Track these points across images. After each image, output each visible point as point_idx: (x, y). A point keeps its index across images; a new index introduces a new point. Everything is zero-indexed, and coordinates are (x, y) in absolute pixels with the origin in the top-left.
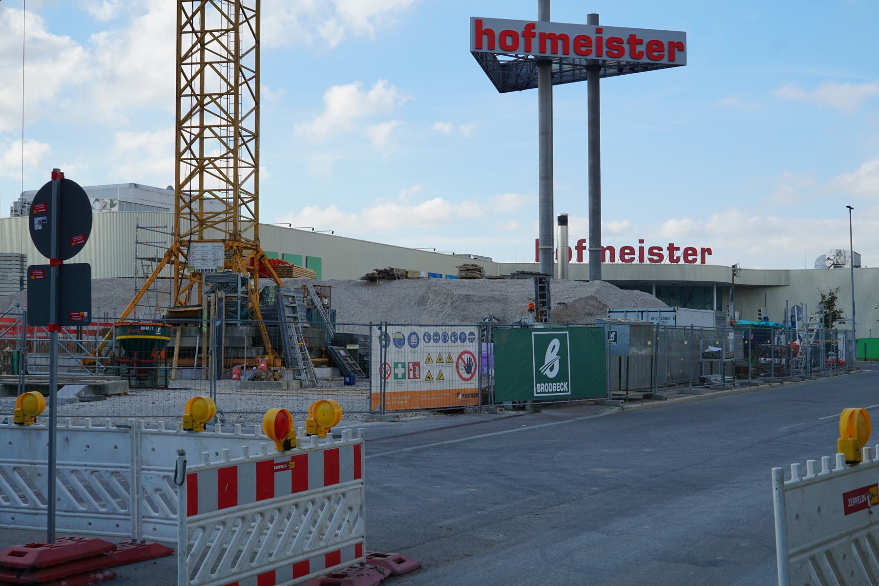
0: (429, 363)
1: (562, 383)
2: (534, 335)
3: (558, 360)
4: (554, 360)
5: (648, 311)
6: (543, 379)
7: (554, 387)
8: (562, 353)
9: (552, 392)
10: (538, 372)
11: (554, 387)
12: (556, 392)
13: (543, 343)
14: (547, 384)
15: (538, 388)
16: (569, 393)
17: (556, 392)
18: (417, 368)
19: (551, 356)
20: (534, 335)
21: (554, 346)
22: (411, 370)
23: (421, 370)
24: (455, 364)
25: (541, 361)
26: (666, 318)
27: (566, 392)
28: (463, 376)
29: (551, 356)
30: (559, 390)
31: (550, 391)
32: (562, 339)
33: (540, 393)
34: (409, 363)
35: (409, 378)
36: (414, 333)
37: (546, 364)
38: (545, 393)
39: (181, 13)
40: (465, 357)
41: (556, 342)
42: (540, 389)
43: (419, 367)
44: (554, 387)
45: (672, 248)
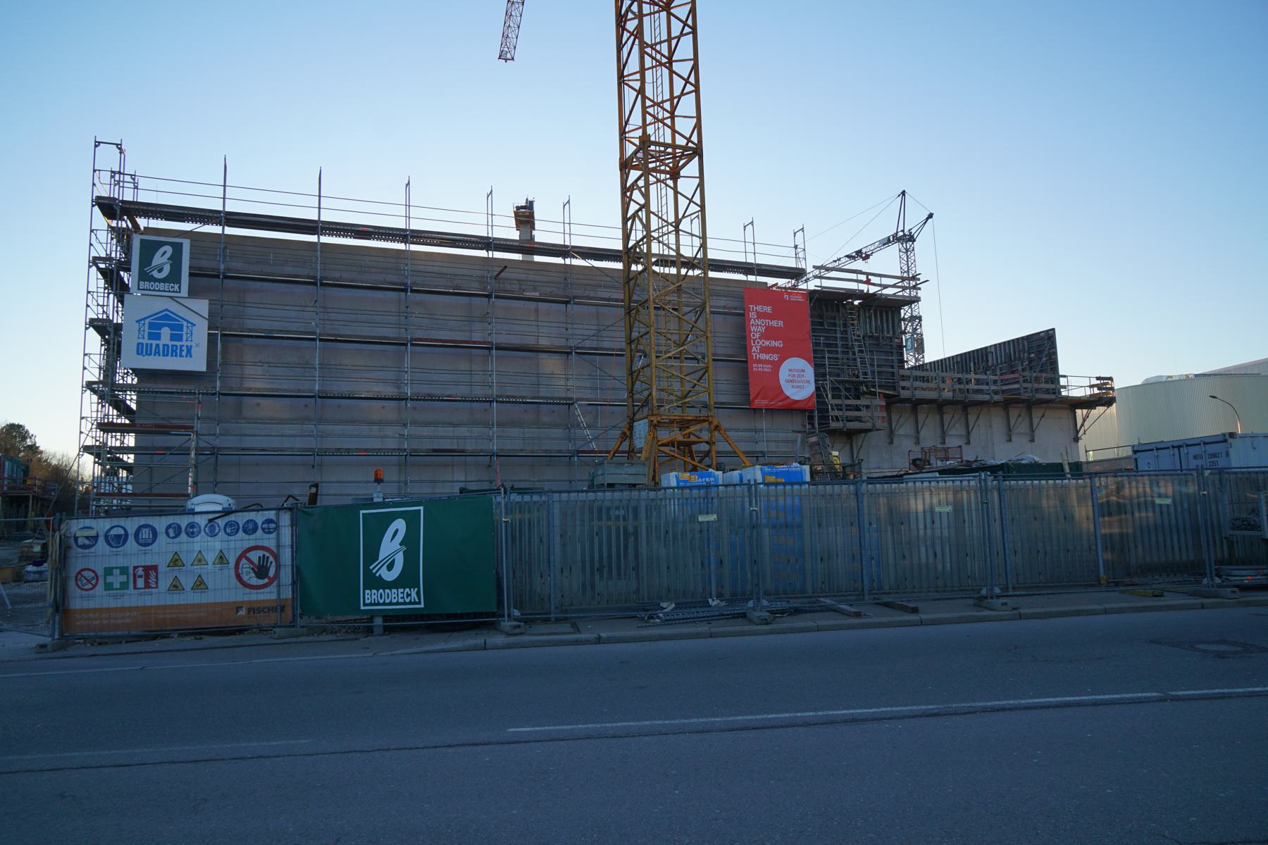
0: (176, 566)
1: (407, 590)
2: (363, 514)
3: (401, 553)
4: (396, 552)
5: (1157, 449)
6: (376, 583)
7: (395, 595)
8: (409, 543)
9: (391, 604)
10: (368, 572)
11: (394, 596)
12: (398, 604)
13: (378, 527)
14: (381, 591)
15: (367, 596)
16: (422, 606)
17: (398, 604)
18: (153, 574)
19: (391, 546)
20: (363, 514)
21: (397, 531)
22: (141, 576)
23: (160, 576)
24: (232, 565)
25: (372, 554)
26: (1214, 455)
27: (415, 603)
28: (245, 578)
29: (391, 546)
30: (402, 601)
31: (387, 601)
32: (411, 519)
33: (370, 604)
34: (135, 568)
35: (135, 588)
36: (146, 526)
37: (380, 559)
38: (379, 604)
39: (646, 221)
40: (255, 556)
41: (400, 525)
42: (370, 597)
43: (157, 573)
44: (395, 595)
45: (159, 355)
